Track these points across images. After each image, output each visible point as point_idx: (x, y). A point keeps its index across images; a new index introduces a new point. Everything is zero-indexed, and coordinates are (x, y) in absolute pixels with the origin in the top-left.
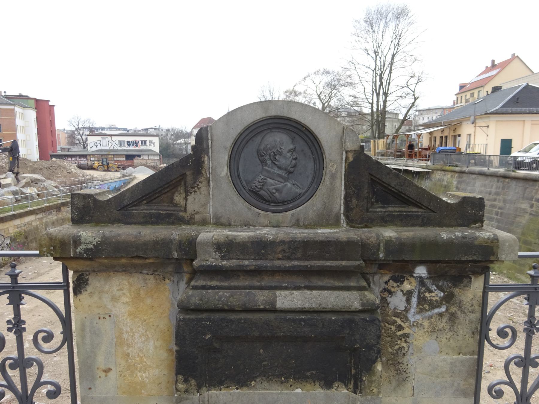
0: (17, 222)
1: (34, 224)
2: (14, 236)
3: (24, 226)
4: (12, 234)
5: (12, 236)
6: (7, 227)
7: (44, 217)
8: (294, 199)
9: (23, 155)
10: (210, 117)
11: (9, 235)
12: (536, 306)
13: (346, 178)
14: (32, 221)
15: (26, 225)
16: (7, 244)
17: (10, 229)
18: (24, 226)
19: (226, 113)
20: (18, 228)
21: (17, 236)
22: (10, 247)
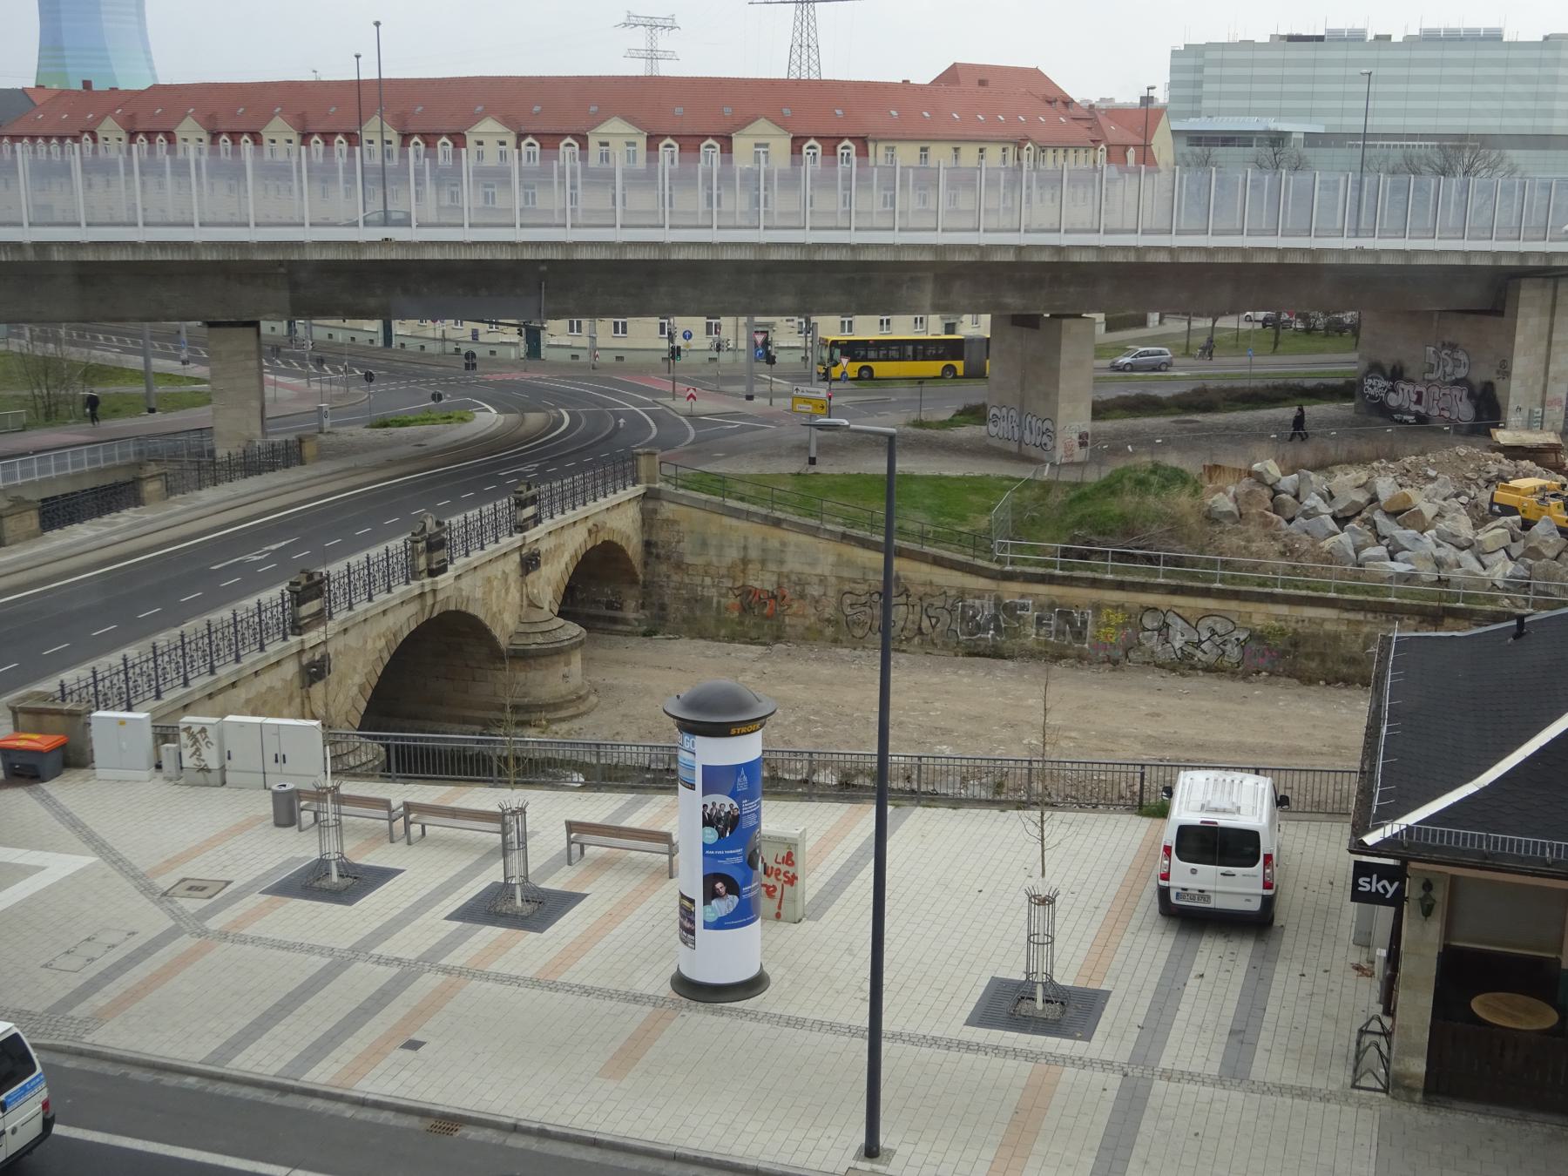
0: (1283, 610)
1: (1328, 627)
2: (1262, 632)
3: (1297, 622)
4: (1259, 628)
5: (1256, 630)
6: (1248, 610)
7: (1368, 622)
8: (556, 706)
9: (579, 330)
10: (1037, 71)
11: (1249, 626)
12: (1505, 39)
13: (1102, 415)
14: (1324, 620)
15: (1303, 621)
16: (1238, 639)
17: (1254, 616)
18: (1297, 622)
19: (1203, 43)
20: (1276, 620)
21: (1269, 633)
22: (1242, 647)
